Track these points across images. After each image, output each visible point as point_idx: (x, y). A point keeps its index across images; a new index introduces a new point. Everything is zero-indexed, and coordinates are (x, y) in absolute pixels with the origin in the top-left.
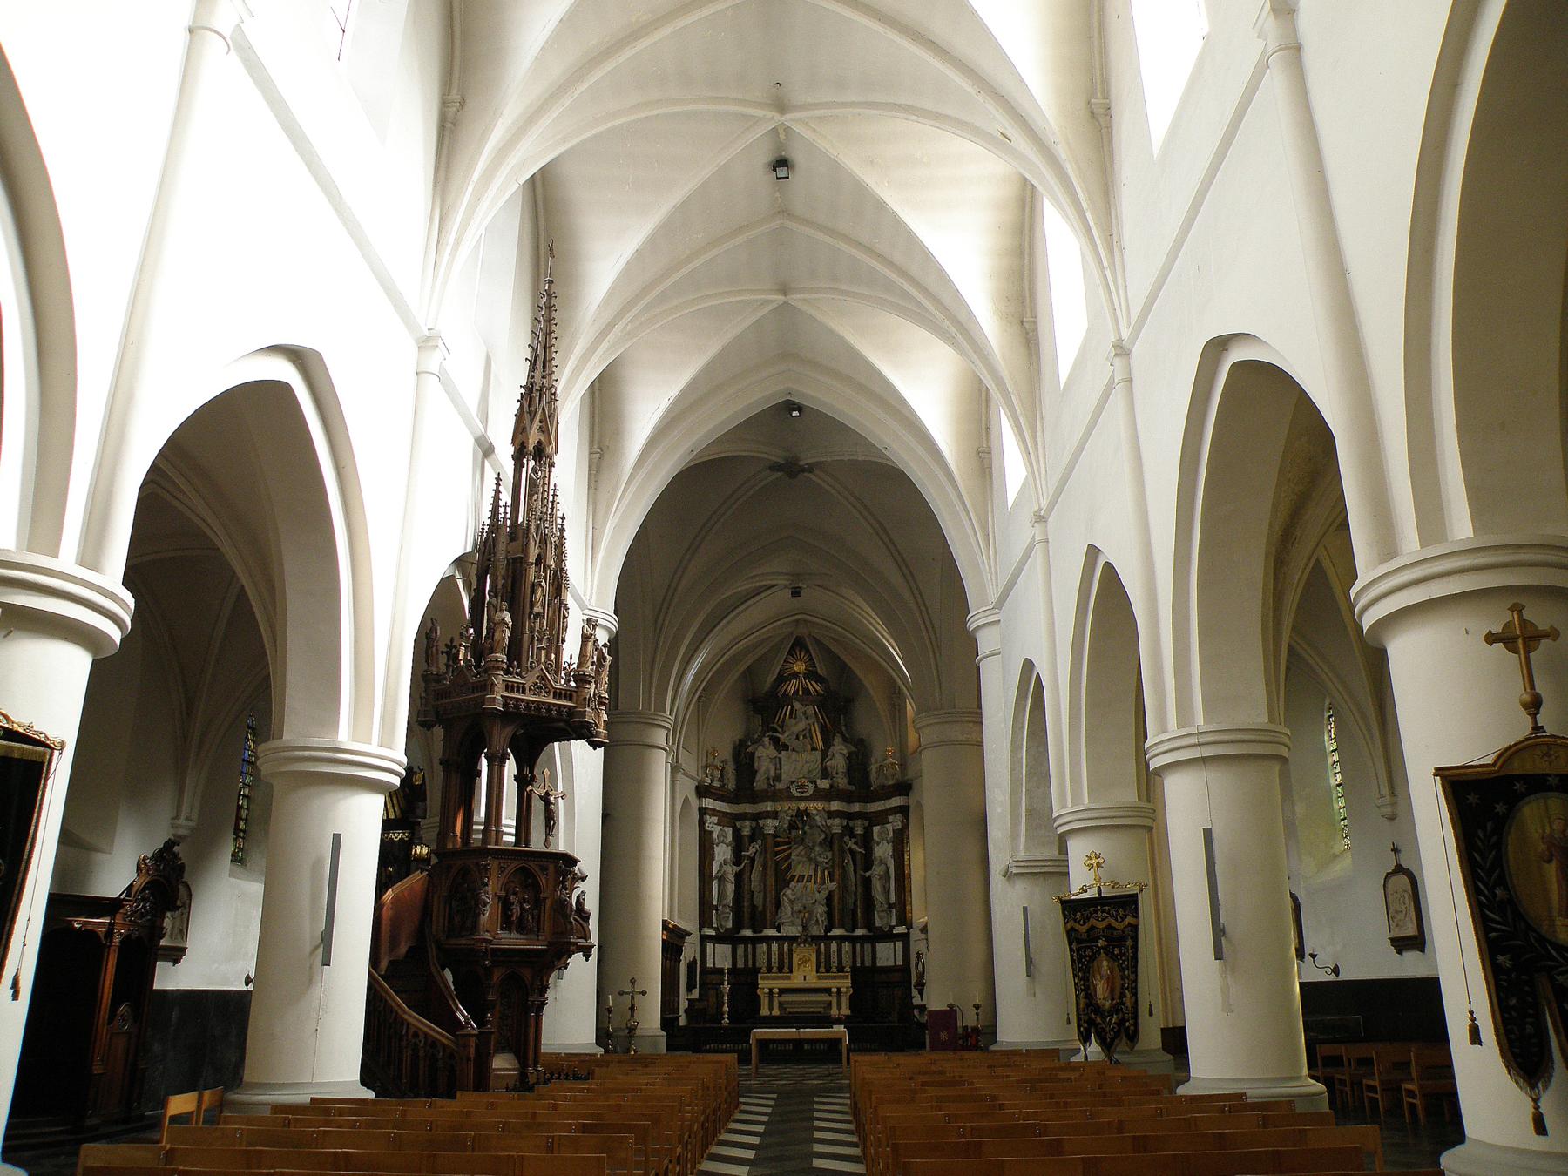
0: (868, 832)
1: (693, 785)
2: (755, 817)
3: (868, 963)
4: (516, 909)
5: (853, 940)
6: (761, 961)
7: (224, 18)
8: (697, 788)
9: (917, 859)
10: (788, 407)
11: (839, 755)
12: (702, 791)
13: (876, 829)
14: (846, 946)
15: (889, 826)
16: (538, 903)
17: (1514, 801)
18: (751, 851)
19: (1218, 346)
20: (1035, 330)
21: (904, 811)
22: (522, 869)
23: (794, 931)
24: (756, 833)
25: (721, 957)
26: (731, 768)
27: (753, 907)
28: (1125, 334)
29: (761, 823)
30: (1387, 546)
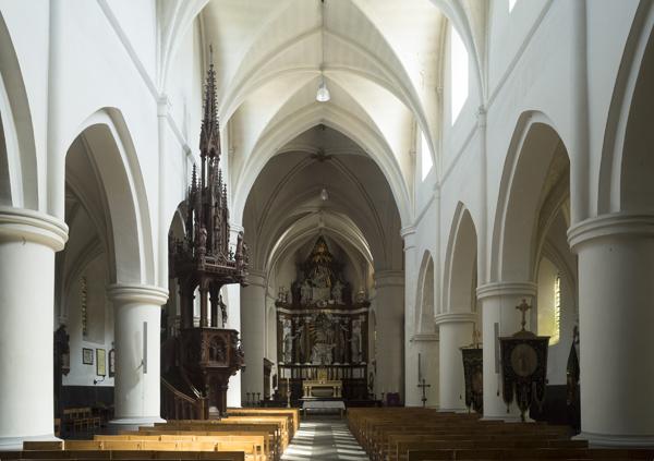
0: (350, 322)
1: (274, 301)
2: (301, 316)
4: (215, 352)
5: (343, 367)
6: (304, 376)
9: (373, 335)
10: (321, 129)
12: (278, 304)
13: (354, 322)
14: (340, 370)
16: (224, 350)
17: (515, 344)
19: (527, 115)
20: (442, 94)
22: (215, 337)
23: (319, 363)
25: (287, 374)
26: (290, 294)
27: (301, 354)
28: (486, 102)
30: (584, 214)
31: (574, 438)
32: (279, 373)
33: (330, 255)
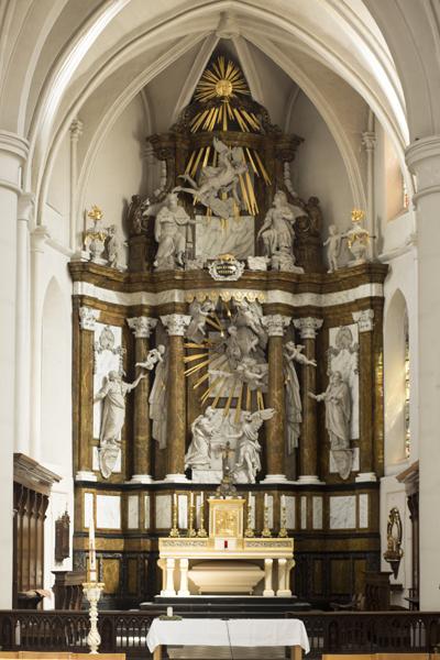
2: (155, 312)
5: (297, 491)
6: (163, 522)
8: (70, 266)
12: (77, 271)
13: (334, 333)
14: (287, 501)
15: (353, 328)
21: (376, 304)
32: (79, 507)
33: (255, 108)
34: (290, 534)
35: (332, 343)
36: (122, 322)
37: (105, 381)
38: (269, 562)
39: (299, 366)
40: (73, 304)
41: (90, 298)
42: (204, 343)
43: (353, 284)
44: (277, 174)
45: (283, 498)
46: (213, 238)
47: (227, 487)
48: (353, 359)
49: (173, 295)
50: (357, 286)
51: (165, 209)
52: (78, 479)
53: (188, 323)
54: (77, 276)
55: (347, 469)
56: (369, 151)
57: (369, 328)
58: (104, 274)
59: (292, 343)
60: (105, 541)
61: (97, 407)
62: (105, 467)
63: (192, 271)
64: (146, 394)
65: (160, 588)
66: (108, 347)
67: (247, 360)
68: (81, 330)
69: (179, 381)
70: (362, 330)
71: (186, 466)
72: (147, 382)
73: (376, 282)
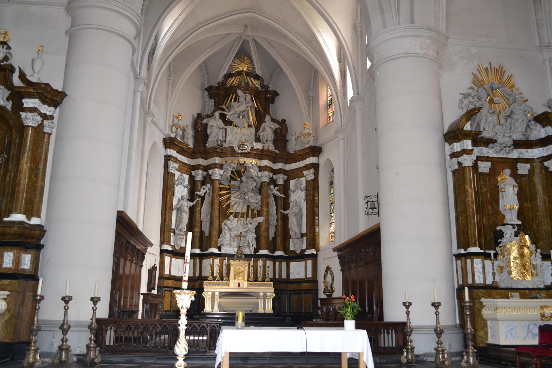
2: (206, 168)
3: (284, 276)
5: (274, 259)
6: (206, 272)
7: (2, 39)
8: (165, 140)
11: (268, 129)
12: (169, 142)
13: (292, 182)
14: (269, 263)
15: (303, 180)
18: (201, 193)
21: (315, 166)
23: (232, 250)
24: (207, 179)
29: (210, 171)
31: (5, 219)
32: (162, 263)
33: (257, 77)
34: (271, 280)
35: (292, 186)
36: (189, 173)
37: (179, 200)
38: (261, 294)
39: (276, 197)
40: (165, 159)
41: (173, 157)
42: (229, 185)
43: (304, 158)
44: (266, 110)
45: (268, 262)
46: (238, 133)
47: (240, 255)
48: (303, 194)
49: (215, 160)
50: (306, 159)
51: (213, 120)
52: (162, 248)
53: (222, 173)
54: (168, 146)
55: (299, 247)
56: (311, 98)
57: (312, 178)
58: (182, 146)
59: (272, 186)
60: (175, 282)
61: (174, 213)
62: (177, 243)
63: (225, 148)
64: (199, 208)
65: (203, 307)
66: (181, 184)
67: (250, 194)
68: (169, 173)
69: (217, 202)
70: (308, 179)
71: (219, 245)
72: (200, 202)
73: (316, 156)
